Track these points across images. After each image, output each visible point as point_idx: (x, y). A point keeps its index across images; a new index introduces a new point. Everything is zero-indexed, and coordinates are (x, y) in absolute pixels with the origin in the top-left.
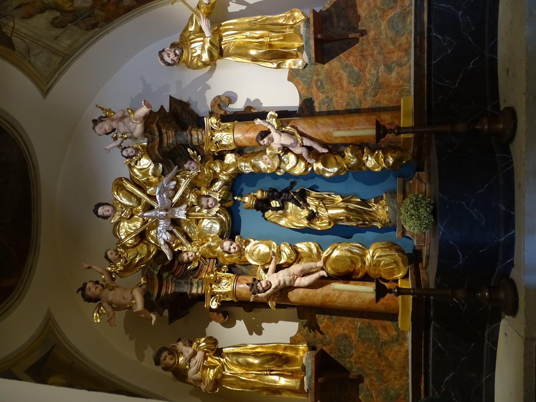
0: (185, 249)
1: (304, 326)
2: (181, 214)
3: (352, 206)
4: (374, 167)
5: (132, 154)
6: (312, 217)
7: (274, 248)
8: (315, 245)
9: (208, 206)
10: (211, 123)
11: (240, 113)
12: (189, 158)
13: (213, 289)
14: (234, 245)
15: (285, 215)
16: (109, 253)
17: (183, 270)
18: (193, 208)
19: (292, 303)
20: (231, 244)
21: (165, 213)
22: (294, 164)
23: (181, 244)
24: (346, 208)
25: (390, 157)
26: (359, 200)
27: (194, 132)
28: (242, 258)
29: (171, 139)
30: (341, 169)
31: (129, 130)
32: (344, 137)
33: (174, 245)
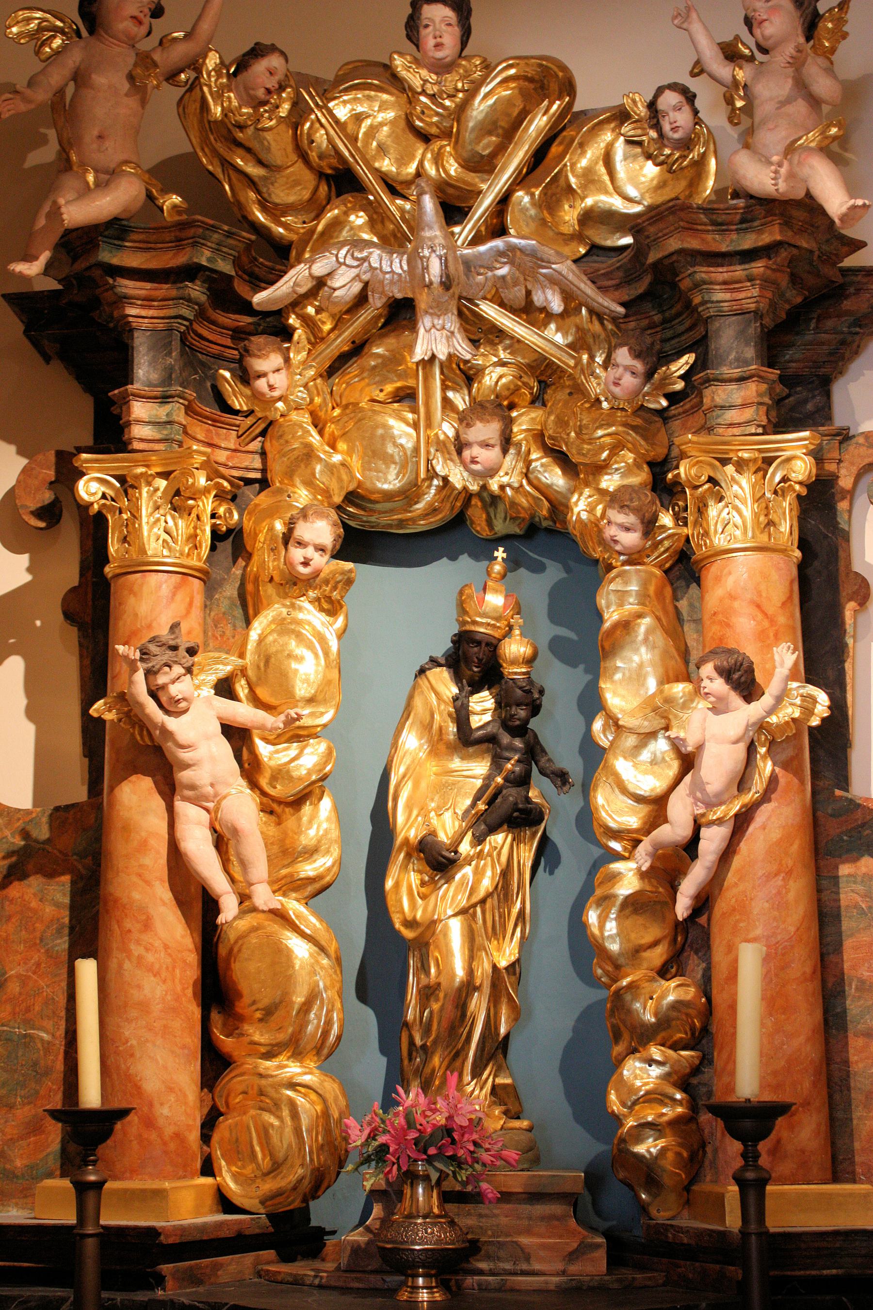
0: (297, 357)
1: (25, 834)
2: (435, 338)
3: (479, 1005)
4: (626, 1089)
5: (666, 127)
6: (439, 862)
7: (312, 714)
8: (329, 870)
9: (468, 445)
10: (789, 460)
11: (841, 554)
12: (655, 359)
13: (149, 484)
14: (319, 560)
15: (438, 747)
16: (274, 61)
17: (215, 349)
18: (460, 380)
19: (112, 789)
20: (321, 549)
21: (436, 280)
22: (631, 788)
23: (316, 338)
24: (469, 986)
25: (661, 1143)
26: (503, 1031)
27: (751, 390)
28: (269, 590)
29: (728, 296)
30: (617, 967)
31: (764, 122)
32: (733, 976)
33: (311, 310)
